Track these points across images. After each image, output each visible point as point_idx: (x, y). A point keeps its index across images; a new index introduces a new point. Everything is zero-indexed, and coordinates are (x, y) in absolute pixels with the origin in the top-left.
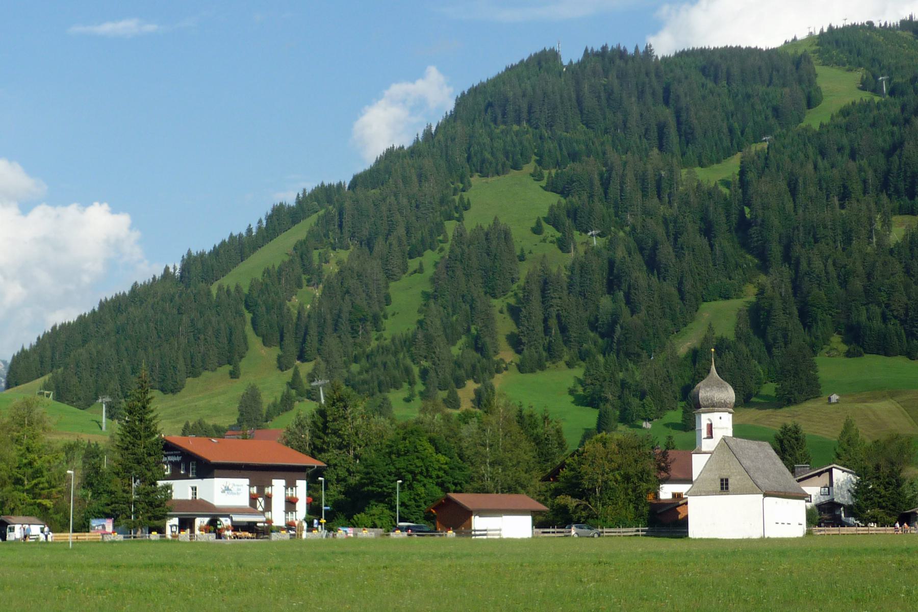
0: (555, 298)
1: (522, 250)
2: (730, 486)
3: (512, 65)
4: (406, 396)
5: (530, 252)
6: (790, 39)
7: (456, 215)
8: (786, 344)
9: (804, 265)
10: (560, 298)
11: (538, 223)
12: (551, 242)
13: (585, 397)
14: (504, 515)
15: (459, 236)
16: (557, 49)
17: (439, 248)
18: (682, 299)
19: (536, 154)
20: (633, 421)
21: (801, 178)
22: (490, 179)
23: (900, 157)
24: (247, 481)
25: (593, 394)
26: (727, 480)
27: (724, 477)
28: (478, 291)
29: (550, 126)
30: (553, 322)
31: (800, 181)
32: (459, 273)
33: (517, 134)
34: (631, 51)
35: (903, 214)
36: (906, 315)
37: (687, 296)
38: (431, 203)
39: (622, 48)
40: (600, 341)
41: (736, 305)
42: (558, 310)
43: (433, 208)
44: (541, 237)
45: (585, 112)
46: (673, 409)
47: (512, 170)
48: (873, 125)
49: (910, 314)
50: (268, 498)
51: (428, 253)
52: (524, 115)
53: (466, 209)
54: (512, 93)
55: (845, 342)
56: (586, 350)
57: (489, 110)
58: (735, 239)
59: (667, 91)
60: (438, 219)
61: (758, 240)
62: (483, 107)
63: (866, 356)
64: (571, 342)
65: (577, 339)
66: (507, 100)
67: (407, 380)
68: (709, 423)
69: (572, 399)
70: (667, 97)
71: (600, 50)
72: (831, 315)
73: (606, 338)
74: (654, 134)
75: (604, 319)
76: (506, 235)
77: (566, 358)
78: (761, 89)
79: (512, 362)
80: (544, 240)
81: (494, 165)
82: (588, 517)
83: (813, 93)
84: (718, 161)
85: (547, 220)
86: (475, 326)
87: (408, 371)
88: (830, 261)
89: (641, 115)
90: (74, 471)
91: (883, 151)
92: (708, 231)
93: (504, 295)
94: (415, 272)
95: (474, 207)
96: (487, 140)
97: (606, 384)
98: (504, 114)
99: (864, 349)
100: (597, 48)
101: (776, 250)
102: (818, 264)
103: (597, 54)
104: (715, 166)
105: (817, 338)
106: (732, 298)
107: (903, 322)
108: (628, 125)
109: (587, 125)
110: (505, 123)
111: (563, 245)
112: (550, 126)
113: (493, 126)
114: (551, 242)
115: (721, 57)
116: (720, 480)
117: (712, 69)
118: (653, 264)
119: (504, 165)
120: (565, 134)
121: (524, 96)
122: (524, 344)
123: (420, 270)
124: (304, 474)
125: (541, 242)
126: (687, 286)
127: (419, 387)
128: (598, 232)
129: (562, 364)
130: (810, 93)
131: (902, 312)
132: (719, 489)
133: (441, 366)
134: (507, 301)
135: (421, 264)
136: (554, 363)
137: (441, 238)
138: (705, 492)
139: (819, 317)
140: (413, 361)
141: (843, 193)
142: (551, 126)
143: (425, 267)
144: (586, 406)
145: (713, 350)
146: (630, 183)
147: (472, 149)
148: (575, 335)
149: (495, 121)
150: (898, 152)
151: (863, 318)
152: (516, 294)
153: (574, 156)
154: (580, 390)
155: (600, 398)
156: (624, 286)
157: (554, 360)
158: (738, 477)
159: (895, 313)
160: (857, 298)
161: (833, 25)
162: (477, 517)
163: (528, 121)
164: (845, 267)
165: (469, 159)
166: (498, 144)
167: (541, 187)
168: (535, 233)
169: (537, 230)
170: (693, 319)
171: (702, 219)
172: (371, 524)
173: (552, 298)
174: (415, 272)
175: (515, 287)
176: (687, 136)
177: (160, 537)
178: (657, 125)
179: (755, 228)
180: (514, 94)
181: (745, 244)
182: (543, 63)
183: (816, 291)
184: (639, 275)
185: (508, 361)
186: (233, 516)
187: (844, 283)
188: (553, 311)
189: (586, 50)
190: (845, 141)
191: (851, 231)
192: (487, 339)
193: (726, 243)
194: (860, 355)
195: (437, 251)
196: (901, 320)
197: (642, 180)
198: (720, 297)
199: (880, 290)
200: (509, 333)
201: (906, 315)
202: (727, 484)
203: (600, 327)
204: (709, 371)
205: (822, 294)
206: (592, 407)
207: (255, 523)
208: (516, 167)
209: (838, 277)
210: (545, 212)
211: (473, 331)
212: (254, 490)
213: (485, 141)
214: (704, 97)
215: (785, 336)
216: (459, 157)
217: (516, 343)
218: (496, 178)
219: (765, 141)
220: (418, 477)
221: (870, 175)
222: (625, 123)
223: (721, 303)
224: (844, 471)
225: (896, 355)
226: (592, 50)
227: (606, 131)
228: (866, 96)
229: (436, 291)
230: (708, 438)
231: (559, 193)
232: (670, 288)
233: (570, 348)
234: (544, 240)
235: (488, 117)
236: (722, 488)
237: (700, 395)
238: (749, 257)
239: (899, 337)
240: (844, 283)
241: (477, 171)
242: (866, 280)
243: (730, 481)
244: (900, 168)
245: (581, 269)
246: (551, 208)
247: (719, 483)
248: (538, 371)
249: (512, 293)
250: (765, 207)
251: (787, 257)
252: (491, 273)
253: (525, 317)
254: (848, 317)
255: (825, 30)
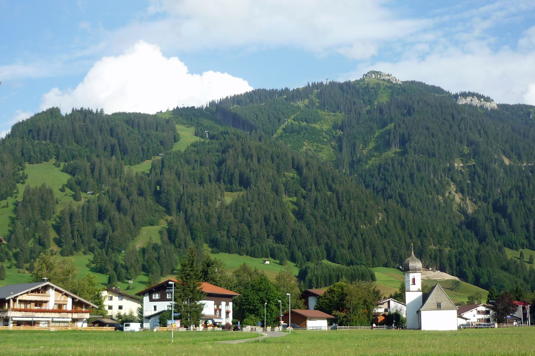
0: (77, 222)
1: (57, 199)
2: (441, 306)
3: (66, 114)
4: (9, 266)
5: (60, 200)
6: (159, 111)
7: (22, 181)
8: (186, 247)
9: (189, 212)
10: (79, 222)
11: (63, 187)
12: (70, 196)
13: (97, 268)
14: (318, 320)
15: (27, 191)
16: (59, 107)
17: (15, 196)
18: (134, 224)
19: (55, 155)
20: (122, 280)
21: (182, 173)
22: (34, 165)
23: (226, 166)
24: (213, 302)
25: (101, 267)
26: (440, 304)
27: (439, 302)
28: (38, 217)
29: (61, 142)
30: (76, 233)
31: (182, 174)
32: (29, 208)
33: (45, 145)
34: (95, 111)
35: (227, 191)
36: (238, 235)
37: (137, 224)
38: (9, 175)
39: (90, 109)
40: (98, 243)
41: (157, 228)
42: (78, 228)
43: (10, 177)
44: (65, 193)
45: (76, 137)
46: (139, 275)
47: (44, 162)
48: (209, 152)
49: (239, 235)
50: (220, 310)
51: (9, 198)
52: (48, 136)
53: (26, 178)
54: (42, 126)
55: (210, 247)
56: (93, 247)
57: (31, 133)
58: (154, 199)
59: (111, 130)
60: (13, 182)
61: (165, 200)
62: (27, 132)
63: (221, 253)
64: (84, 242)
65: (88, 241)
66: (40, 129)
67: (7, 258)
68: (413, 278)
69: (88, 269)
70: (112, 132)
71: (80, 109)
72: (203, 234)
73: (101, 242)
74: (109, 149)
75: (100, 232)
76: (51, 192)
77: (83, 250)
78: (154, 133)
79: (57, 251)
80: (66, 195)
81: (36, 158)
82: (346, 321)
83: (176, 136)
84: (138, 163)
85: (66, 186)
86: (38, 234)
87: (7, 254)
88: (201, 210)
89: (103, 140)
90: (291, 294)
91: (215, 163)
92: (141, 194)
93: (50, 219)
94: (4, 207)
95: (29, 178)
96: (31, 147)
97: (108, 262)
98: (38, 135)
99: (220, 250)
100: (79, 108)
101: (174, 205)
102: (196, 211)
103: (77, 111)
104: (137, 166)
105: (198, 245)
106: (155, 225)
107: (236, 239)
108: (97, 144)
109: (77, 143)
110: (39, 140)
111: (76, 198)
112: (61, 142)
113: (33, 140)
114: (70, 196)
115: (134, 116)
116: (436, 304)
117: (131, 122)
118: (119, 208)
119: (41, 159)
120: (68, 146)
121: (48, 127)
122: (63, 243)
123: (7, 206)
124: (231, 299)
125: (65, 195)
126: (137, 219)
127: (14, 261)
128: (92, 192)
129: (81, 252)
130: (175, 136)
131: (236, 234)
132: (436, 308)
133: (25, 252)
134: (51, 222)
135: (7, 203)
136: (77, 252)
137: (15, 191)
138: (429, 309)
139: (198, 235)
140: (9, 249)
141: (201, 181)
142: (61, 142)
143: (9, 205)
144: (97, 272)
145: (412, 244)
146: (104, 172)
147: (24, 151)
148: (87, 239)
149: (33, 138)
150: (224, 164)
151: (219, 236)
152: (55, 219)
153: (73, 157)
154: (93, 266)
155: (105, 269)
156: (107, 218)
157: (77, 251)
158: (445, 302)
159: (233, 235)
160: (215, 227)
161: (179, 106)
162: (308, 321)
163: (50, 139)
164: (208, 213)
165: (23, 155)
166: (37, 149)
167: (60, 170)
168: (61, 191)
169: (62, 190)
170: (139, 234)
171: (138, 189)
172: (253, 324)
173: (75, 222)
174: (4, 207)
175: (54, 216)
176: (124, 151)
177: (187, 329)
178: (110, 145)
179: (164, 194)
180: (43, 127)
181: (158, 201)
182: (54, 113)
183: (196, 223)
184: (114, 213)
185: (56, 250)
186: (215, 319)
187: (208, 221)
188: (76, 228)
189: (73, 109)
190: (198, 158)
191: (207, 197)
192: (46, 240)
193: (150, 201)
194: (218, 253)
195: (14, 197)
196: (235, 238)
197: (109, 170)
198: (150, 224)
199: (224, 224)
200: (54, 237)
201: (238, 235)
202: (440, 305)
203: (97, 236)
204: (411, 254)
205: (199, 224)
206: (101, 273)
207: (17, 326)
208: (46, 160)
209: (205, 217)
210: (65, 182)
211: (37, 236)
212: (216, 307)
213: (30, 147)
214: (129, 135)
215: (185, 243)
216: (18, 154)
217: (59, 243)
218: (37, 165)
219: (160, 156)
220: (271, 301)
221: (212, 174)
222: (96, 143)
223: (150, 227)
224: (395, 301)
225: (234, 253)
226: (76, 109)
227: (87, 146)
228: (198, 139)
229: (17, 216)
230: (412, 284)
231: (69, 173)
232: (128, 219)
233: (84, 246)
234: (66, 195)
235: (30, 137)
236: (438, 307)
237: (410, 265)
238: (160, 207)
239: (235, 245)
240: (208, 221)
241: (27, 161)
242: (217, 220)
243: (442, 304)
244: (226, 171)
245: (86, 209)
246: (69, 180)
247: (436, 305)
248: (70, 255)
249: (54, 219)
250: (168, 185)
251: (179, 209)
252: (44, 209)
253: (64, 230)
254: (210, 236)
255: (175, 108)
